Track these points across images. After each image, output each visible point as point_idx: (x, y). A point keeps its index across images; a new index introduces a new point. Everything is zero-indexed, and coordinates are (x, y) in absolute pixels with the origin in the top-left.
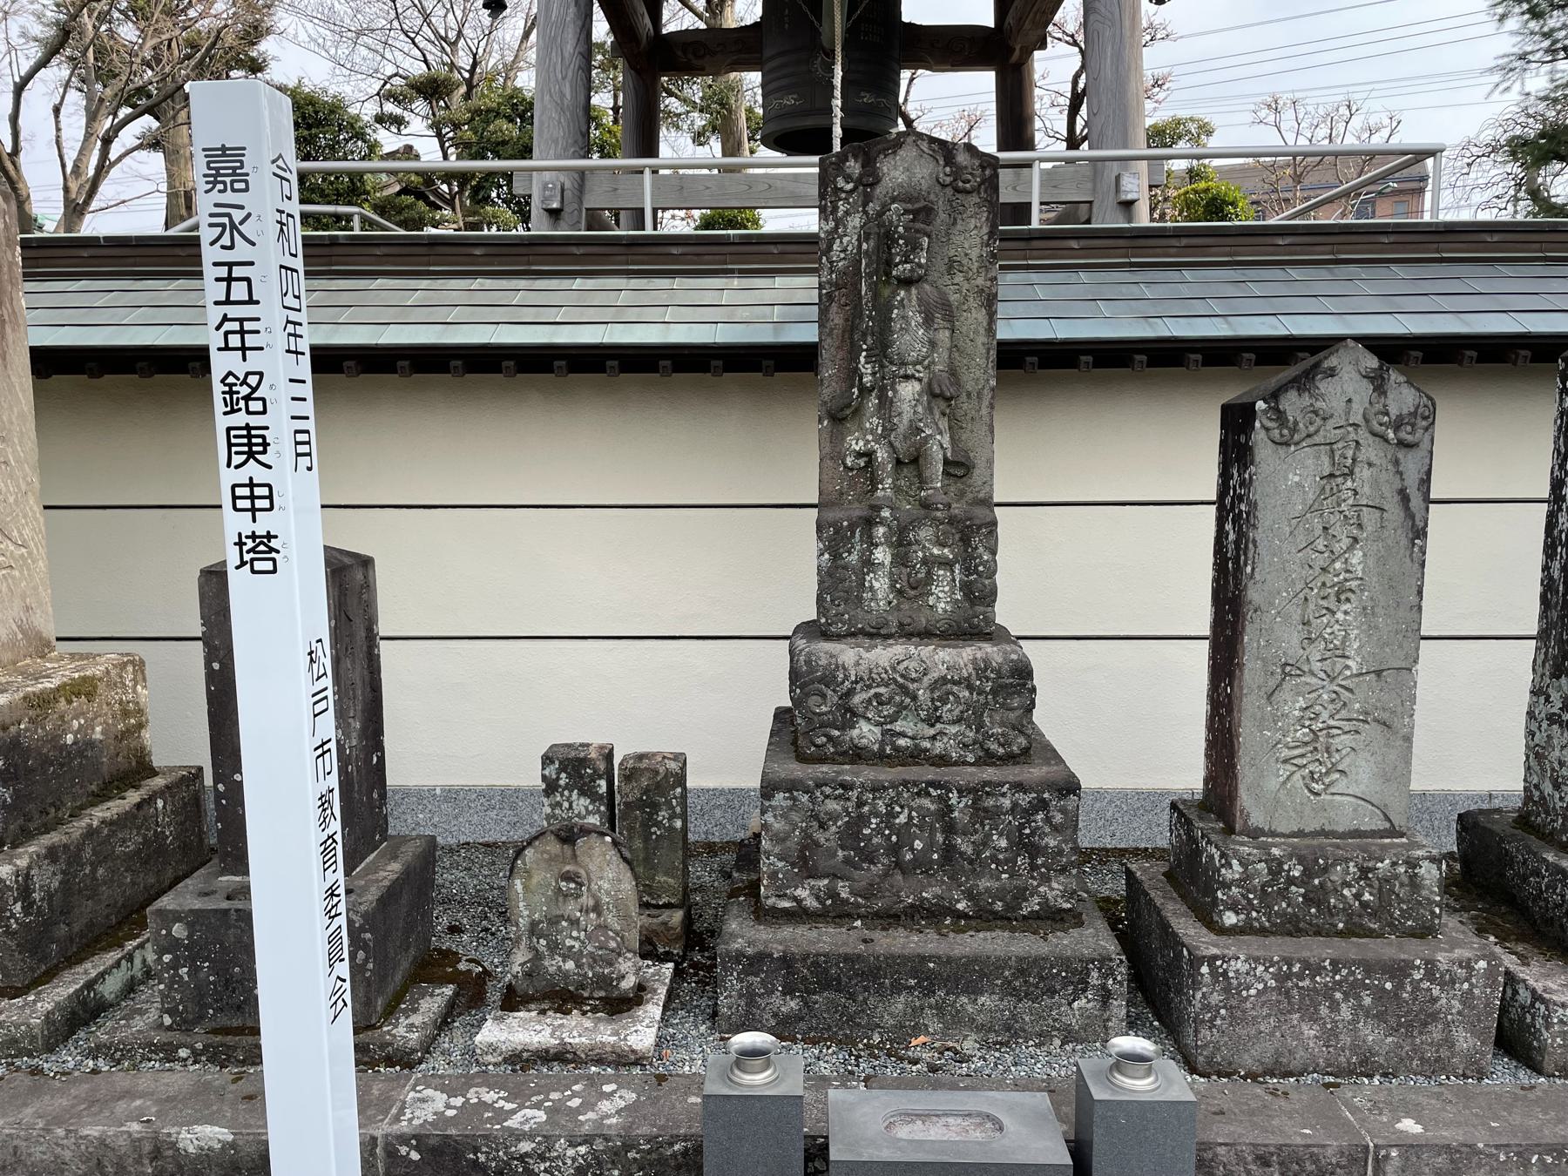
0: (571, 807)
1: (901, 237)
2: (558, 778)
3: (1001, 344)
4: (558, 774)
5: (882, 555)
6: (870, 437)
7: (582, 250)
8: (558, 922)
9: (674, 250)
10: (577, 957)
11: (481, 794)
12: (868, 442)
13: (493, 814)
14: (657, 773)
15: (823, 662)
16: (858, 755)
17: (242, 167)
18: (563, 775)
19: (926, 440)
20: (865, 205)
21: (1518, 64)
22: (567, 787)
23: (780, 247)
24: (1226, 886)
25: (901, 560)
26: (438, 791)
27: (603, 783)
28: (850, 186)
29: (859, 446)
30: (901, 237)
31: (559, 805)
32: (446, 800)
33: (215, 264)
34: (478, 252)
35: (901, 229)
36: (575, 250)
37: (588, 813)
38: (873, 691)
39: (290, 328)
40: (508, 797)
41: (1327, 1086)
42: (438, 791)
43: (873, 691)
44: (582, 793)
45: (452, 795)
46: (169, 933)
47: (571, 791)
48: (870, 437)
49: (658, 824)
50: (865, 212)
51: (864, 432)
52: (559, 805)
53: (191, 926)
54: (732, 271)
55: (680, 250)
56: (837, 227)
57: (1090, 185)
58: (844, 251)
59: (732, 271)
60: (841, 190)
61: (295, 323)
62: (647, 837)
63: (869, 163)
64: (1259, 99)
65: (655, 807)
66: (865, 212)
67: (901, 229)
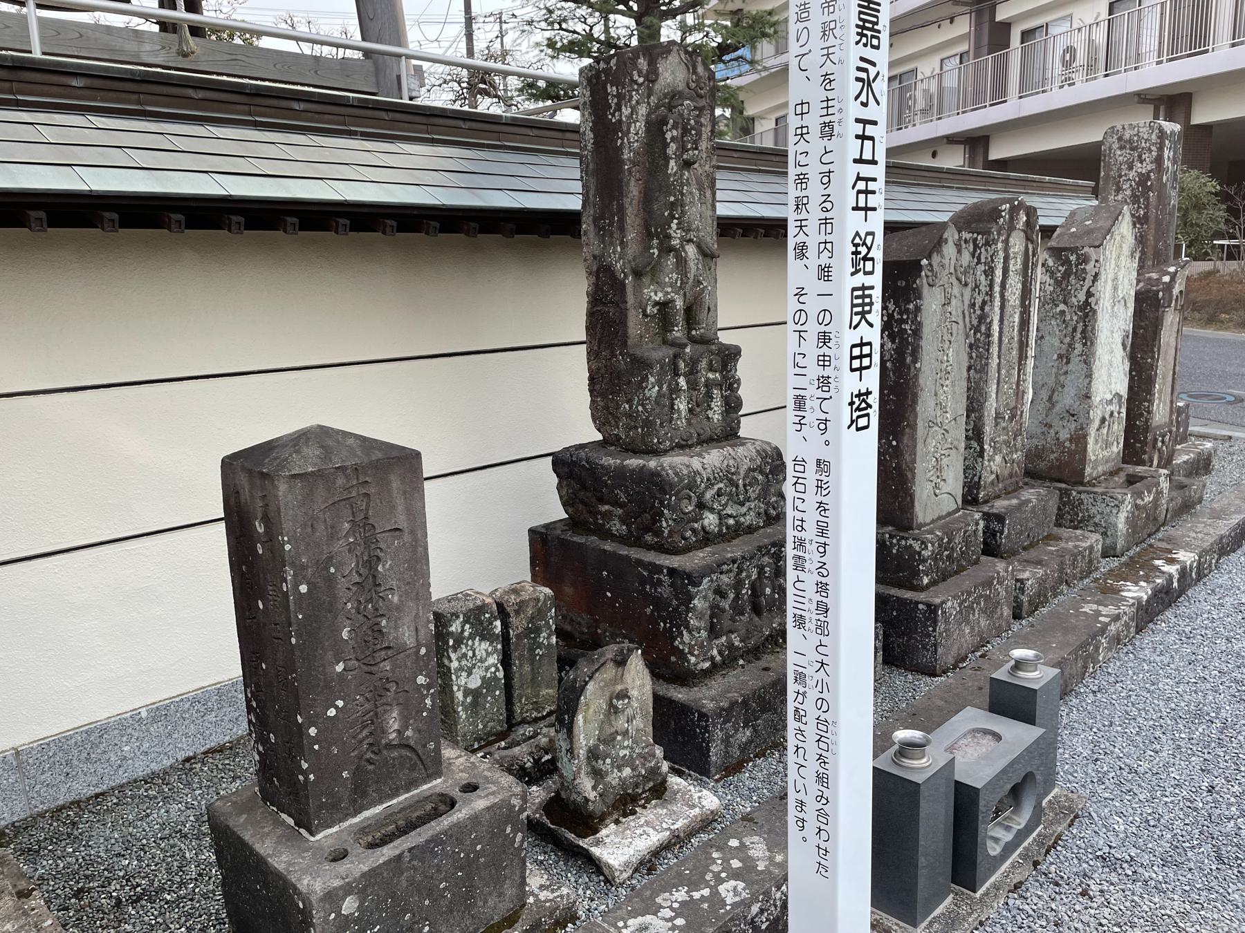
0: (474, 655)
1: (693, 128)
2: (463, 631)
3: (719, 218)
4: (463, 627)
5: (682, 382)
6: (669, 290)
7: (201, 94)
8: (615, 739)
9: (296, 106)
10: (629, 762)
11: (195, 701)
12: (667, 293)
13: (211, 717)
14: (538, 600)
15: (685, 472)
16: (707, 539)
17: (877, 23)
18: (467, 626)
19: (702, 291)
20: (649, 97)
21: (527, 28)
22: (472, 637)
23: (391, 114)
24: (925, 561)
25: (693, 386)
26: (144, 714)
27: (498, 623)
28: (641, 80)
29: (659, 297)
30: (693, 128)
31: (465, 655)
32: (154, 720)
33: (858, 121)
34: (75, 82)
35: (692, 122)
36: (191, 93)
37: (488, 654)
38: (716, 487)
39: (861, 185)
40: (202, 702)
41: (982, 656)
42: (144, 714)
43: (716, 487)
44: (483, 638)
45: (161, 713)
46: (339, 914)
47: (474, 640)
48: (669, 290)
49: (540, 646)
50: (649, 103)
51: (661, 285)
52: (465, 655)
53: (362, 894)
54: (355, 133)
55: (302, 106)
56: (632, 114)
57: (374, 79)
58: (637, 134)
59: (355, 133)
60: (636, 82)
61: (867, 180)
62: (532, 661)
63: (652, 63)
64: (275, 13)
65: (537, 631)
66: (649, 103)
67: (692, 122)
